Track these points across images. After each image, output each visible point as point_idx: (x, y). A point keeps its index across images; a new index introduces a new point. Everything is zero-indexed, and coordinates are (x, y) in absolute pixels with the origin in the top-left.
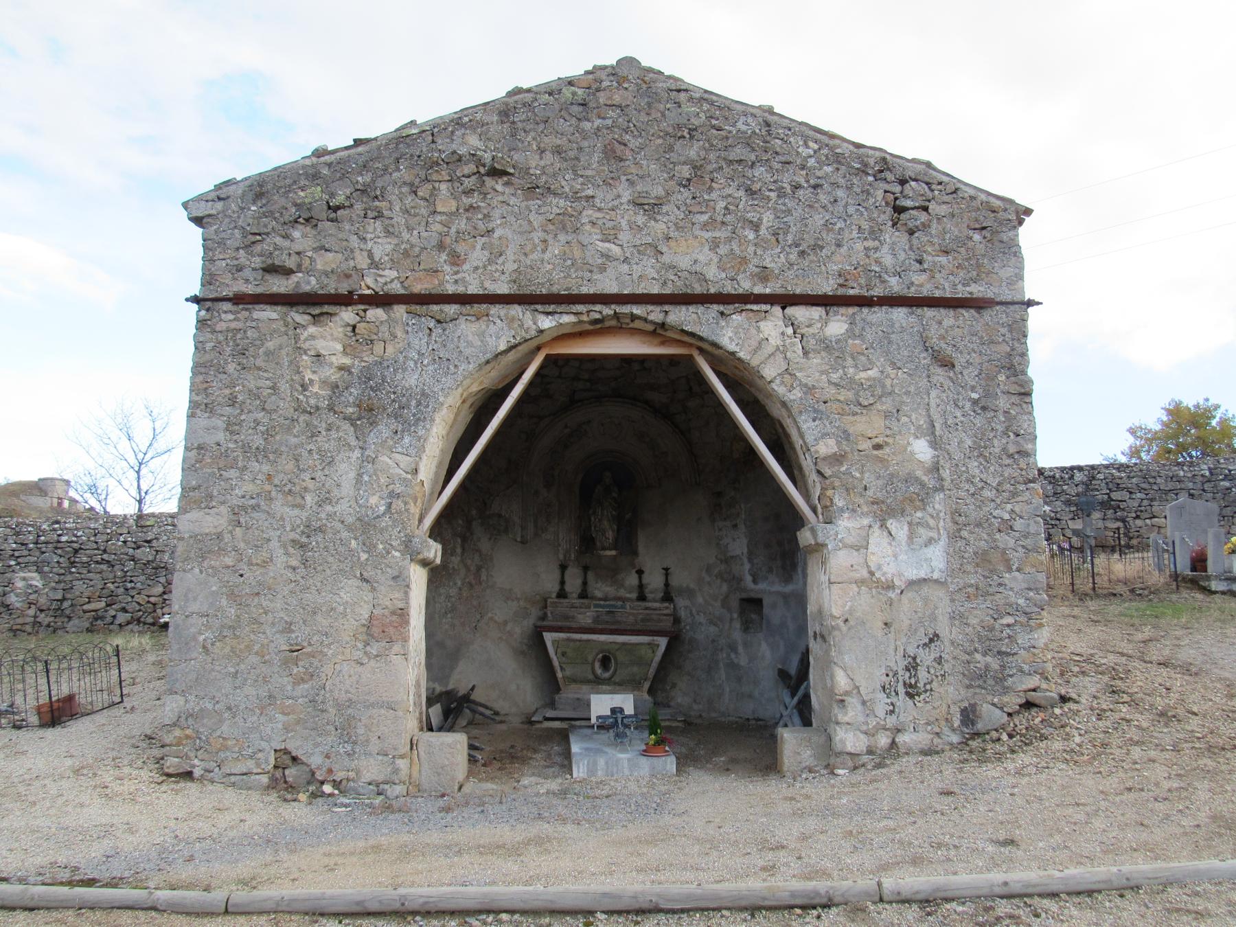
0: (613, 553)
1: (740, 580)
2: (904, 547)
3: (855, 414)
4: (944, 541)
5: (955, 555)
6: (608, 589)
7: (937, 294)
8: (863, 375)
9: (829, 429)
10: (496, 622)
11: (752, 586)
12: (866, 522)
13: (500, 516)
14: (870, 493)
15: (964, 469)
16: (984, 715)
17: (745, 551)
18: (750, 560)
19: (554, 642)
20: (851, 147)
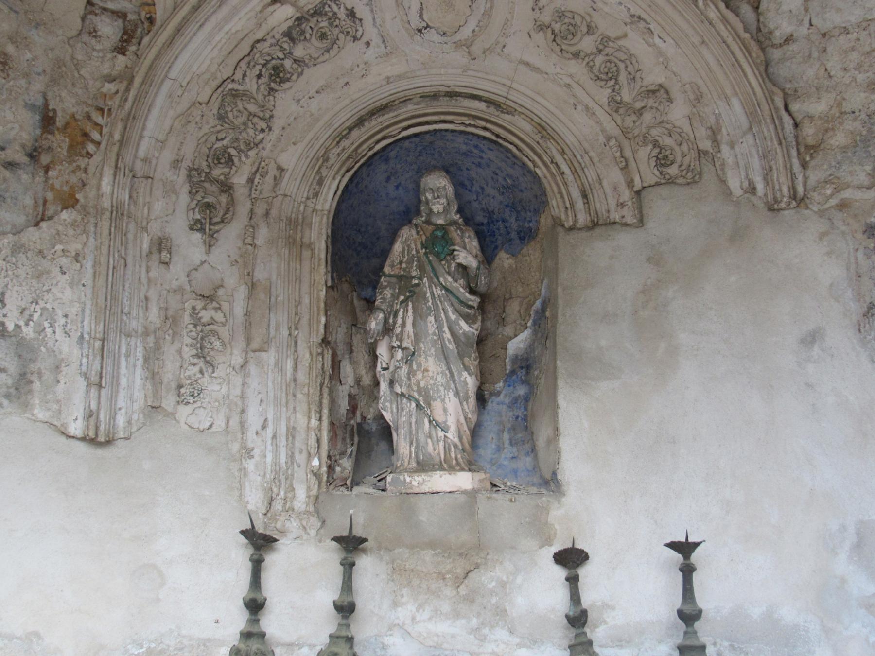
0: (464, 480)
6: (443, 627)
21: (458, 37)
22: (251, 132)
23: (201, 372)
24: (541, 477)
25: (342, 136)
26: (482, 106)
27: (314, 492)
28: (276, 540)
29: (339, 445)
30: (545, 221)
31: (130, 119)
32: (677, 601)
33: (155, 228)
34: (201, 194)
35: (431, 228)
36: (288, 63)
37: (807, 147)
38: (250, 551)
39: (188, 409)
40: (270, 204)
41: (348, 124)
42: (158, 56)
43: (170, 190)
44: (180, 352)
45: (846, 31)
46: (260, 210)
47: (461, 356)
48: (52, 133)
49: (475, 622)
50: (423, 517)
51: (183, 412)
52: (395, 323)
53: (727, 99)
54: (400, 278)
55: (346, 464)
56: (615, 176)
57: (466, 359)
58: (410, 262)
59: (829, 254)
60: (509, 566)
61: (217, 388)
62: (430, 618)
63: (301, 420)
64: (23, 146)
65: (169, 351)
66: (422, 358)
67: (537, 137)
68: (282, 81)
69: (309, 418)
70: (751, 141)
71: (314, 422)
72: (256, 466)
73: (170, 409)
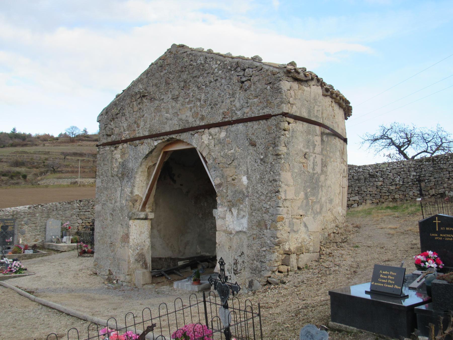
2: (235, 219)
3: (227, 167)
4: (247, 216)
5: (250, 222)
7: (253, 115)
8: (230, 152)
9: (218, 174)
12: (225, 209)
14: (228, 198)
15: (256, 188)
16: (255, 284)
20: (230, 59)
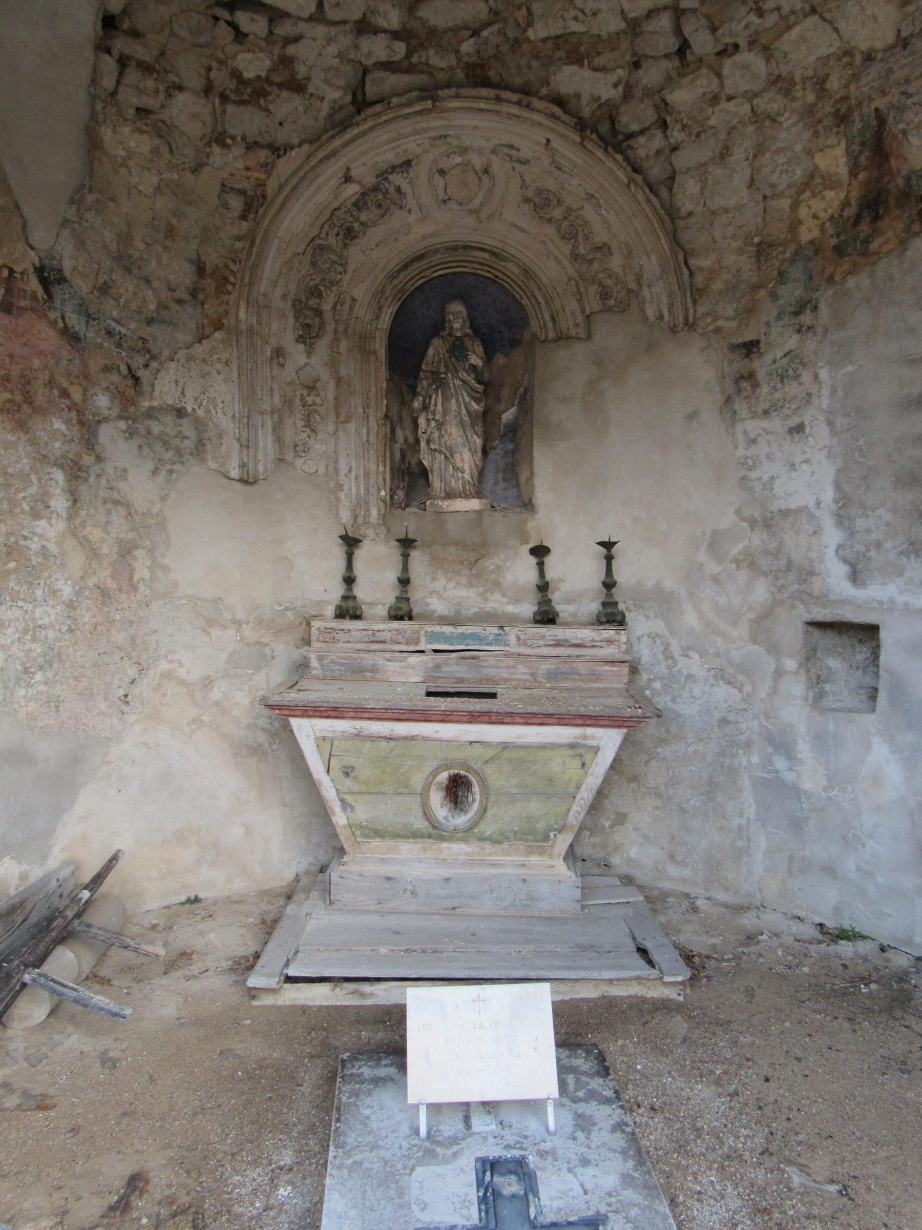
0: (474, 504)
1: (808, 573)
6: (463, 593)
10: (182, 682)
11: (847, 590)
13: (180, 413)
17: (828, 495)
18: (841, 519)
19: (321, 741)
21: (471, 206)
22: (333, 274)
23: (309, 436)
24: (523, 502)
25: (392, 277)
26: (486, 255)
27: (383, 511)
28: (361, 541)
29: (396, 482)
30: (527, 335)
31: (255, 267)
32: (602, 576)
33: (274, 341)
34: (302, 317)
35: (453, 339)
36: (356, 225)
37: (698, 290)
38: (345, 548)
39: (302, 461)
40: (348, 325)
41: (397, 268)
42: (271, 221)
43: (283, 316)
44: (294, 424)
45: (726, 211)
46: (341, 328)
47: (473, 425)
48: (204, 278)
49: (481, 589)
50: (450, 527)
51: (299, 462)
52: (430, 403)
53: (648, 256)
54: (432, 372)
55: (401, 494)
56: (574, 305)
57: (476, 427)
58: (439, 362)
59: (706, 362)
60: (502, 556)
61: (319, 447)
62: (455, 588)
63: (373, 467)
64: (187, 288)
65: (288, 422)
66: (448, 428)
67: (523, 278)
68: (353, 238)
69: (378, 466)
70: (662, 284)
71: (381, 468)
72: (346, 495)
73: (290, 460)
